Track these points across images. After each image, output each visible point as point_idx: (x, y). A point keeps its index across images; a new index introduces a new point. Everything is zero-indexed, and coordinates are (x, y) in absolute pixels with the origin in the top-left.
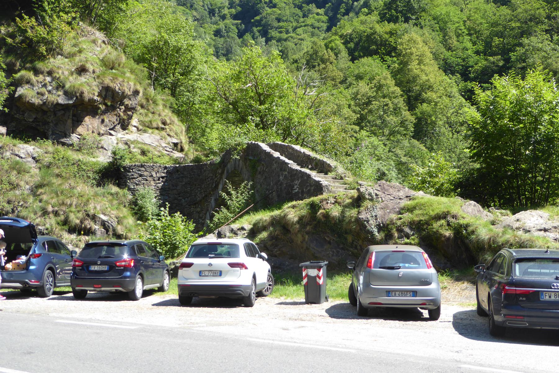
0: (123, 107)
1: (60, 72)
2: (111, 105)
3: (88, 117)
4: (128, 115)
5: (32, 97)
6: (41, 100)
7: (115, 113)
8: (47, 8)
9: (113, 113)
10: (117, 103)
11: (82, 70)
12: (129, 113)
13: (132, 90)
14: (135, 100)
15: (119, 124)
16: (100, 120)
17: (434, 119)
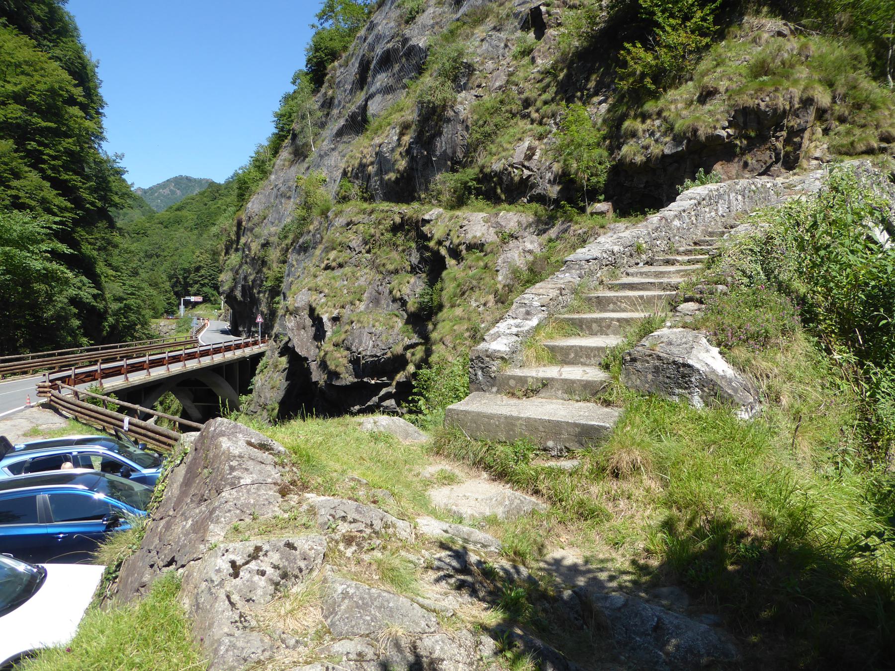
0: (784, 133)
1: (673, 107)
2: (757, 135)
3: (720, 163)
4: (795, 143)
5: (634, 155)
6: (645, 156)
7: (767, 146)
8: (660, 20)
9: (763, 148)
10: (769, 129)
11: (707, 95)
12: (795, 140)
13: (797, 100)
14: (806, 115)
15: (776, 162)
16: (742, 163)
17: (558, 215)
